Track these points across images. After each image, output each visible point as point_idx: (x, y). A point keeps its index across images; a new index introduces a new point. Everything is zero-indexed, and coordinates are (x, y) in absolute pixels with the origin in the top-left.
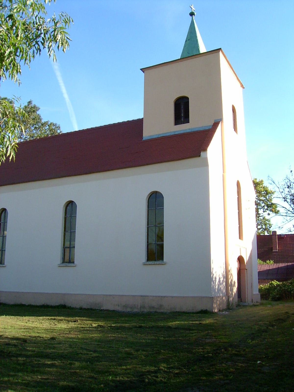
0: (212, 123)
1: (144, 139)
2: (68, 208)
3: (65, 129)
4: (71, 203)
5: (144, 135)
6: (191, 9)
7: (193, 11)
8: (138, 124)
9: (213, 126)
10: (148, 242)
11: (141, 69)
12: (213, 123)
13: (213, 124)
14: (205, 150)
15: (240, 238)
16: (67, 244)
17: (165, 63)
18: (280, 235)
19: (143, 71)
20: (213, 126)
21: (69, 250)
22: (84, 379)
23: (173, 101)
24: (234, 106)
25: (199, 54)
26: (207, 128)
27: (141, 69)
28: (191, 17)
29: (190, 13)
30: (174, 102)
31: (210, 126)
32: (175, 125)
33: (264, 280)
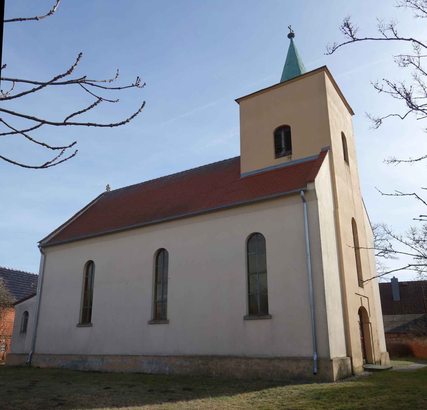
0: (318, 152)
1: (242, 177)
2: (160, 257)
3: (1, 70)
4: (162, 252)
5: (242, 172)
6: (290, 29)
7: (292, 32)
8: (236, 161)
9: (320, 155)
10: (249, 292)
11: (236, 100)
12: (320, 151)
13: (320, 153)
14: (312, 181)
15: (359, 286)
16: (159, 298)
17: (262, 90)
18: (402, 282)
19: (239, 102)
20: (320, 155)
21: (394, 299)
22: (241, 401)
23: (273, 132)
24: (344, 132)
25: (299, 75)
26: (314, 159)
27: (236, 100)
28: (290, 40)
29: (287, 35)
30: (273, 132)
31: (317, 155)
32: (276, 158)
33: (389, 334)
